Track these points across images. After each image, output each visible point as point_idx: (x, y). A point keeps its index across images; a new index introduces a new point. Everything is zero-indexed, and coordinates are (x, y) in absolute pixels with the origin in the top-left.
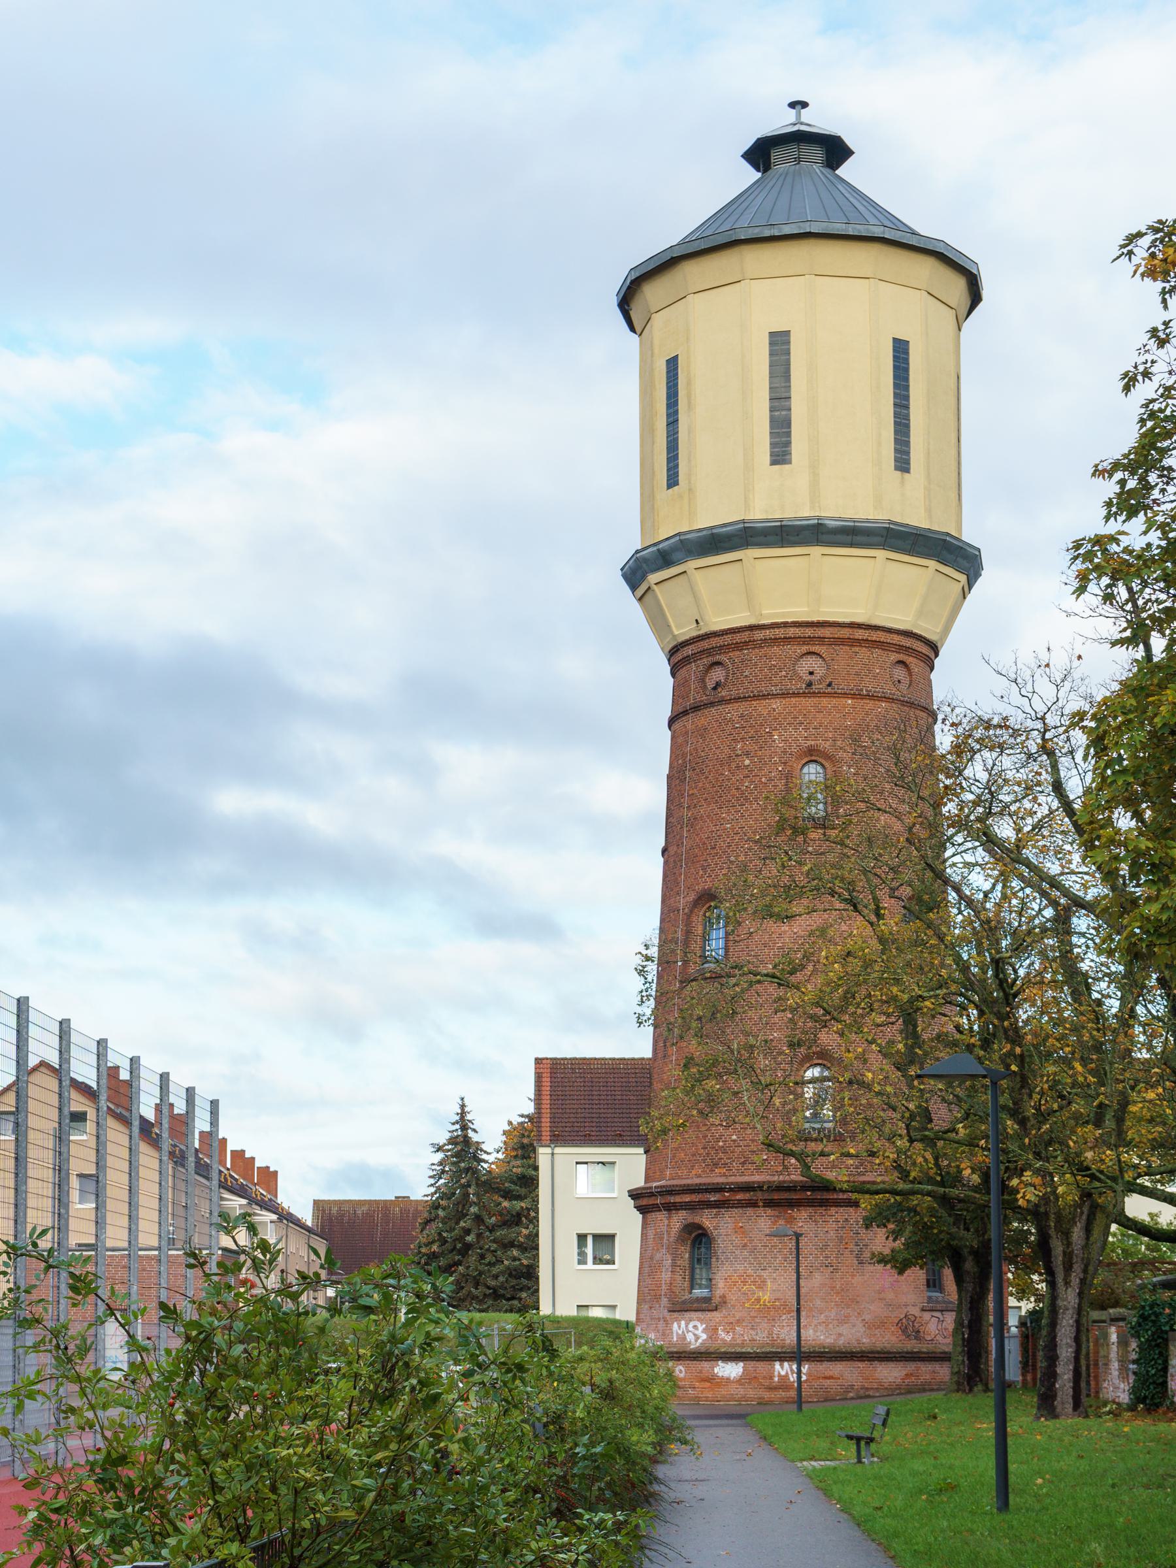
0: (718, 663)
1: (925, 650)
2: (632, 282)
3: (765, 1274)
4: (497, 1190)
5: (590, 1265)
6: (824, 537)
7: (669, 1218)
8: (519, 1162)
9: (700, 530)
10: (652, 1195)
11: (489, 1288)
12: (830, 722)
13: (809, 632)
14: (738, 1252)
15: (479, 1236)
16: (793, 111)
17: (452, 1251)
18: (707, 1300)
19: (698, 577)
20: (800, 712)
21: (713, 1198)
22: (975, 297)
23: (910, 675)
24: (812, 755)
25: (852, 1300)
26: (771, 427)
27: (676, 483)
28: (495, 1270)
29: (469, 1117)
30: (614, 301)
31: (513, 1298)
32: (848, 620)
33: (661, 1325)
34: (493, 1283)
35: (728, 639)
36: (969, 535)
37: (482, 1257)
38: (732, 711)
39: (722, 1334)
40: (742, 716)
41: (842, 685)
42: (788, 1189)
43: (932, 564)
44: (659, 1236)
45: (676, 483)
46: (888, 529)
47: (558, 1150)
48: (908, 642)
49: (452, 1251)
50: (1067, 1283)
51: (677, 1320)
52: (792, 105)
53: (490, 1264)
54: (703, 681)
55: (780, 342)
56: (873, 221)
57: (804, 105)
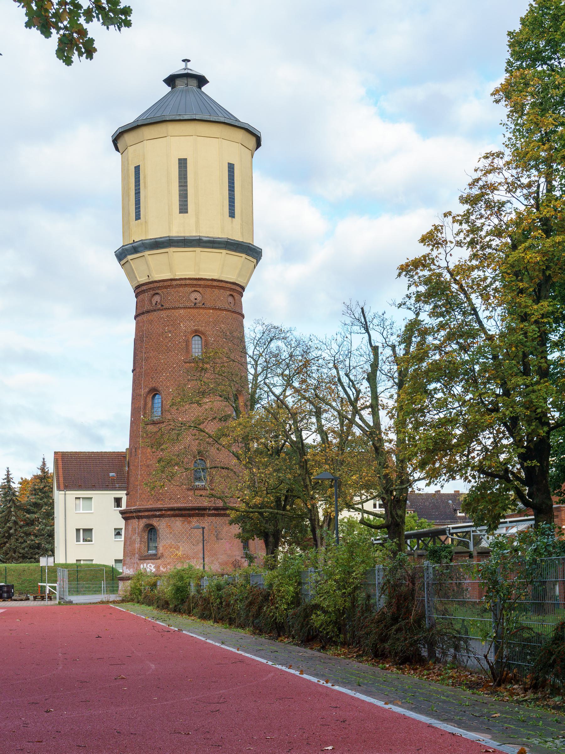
0: (157, 294)
1: (240, 289)
2: (120, 133)
3: (179, 544)
4: (24, 510)
5: (81, 542)
6: (202, 244)
7: (138, 522)
8: (34, 497)
9: (151, 239)
10: (131, 512)
11: (20, 553)
12: (204, 320)
13: (195, 282)
14: (168, 535)
15: (16, 530)
16: (184, 63)
17: (3, 537)
18: (155, 555)
19: (150, 258)
20: (191, 315)
21: (158, 513)
22: (258, 144)
23: (235, 300)
24: (197, 333)
25: (214, 554)
26: (179, 198)
27: (139, 218)
28: (23, 546)
29: (11, 476)
30: (111, 140)
31: (31, 558)
32: (210, 278)
33: (135, 565)
34: (22, 551)
35: (161, 284)
36: (257, 243)
37: (17, 540)
38: (163, 314)
39: (162, 569)
40: (168, 316)
41: (208, 305)
42: (189, 510)
43: (244, 256)
44: (134, 530)
45: (139, 218)
46: (227, 241)
47: (67, 492)
48: (234, 287)
49: (3, 537)
50: (322, 544)
51: (142, 563)
52: (184, 61)
53: (21, 543)
54: (151, 301)
55: (183, 163)
56: (220, 115)
57: (189, 61)
